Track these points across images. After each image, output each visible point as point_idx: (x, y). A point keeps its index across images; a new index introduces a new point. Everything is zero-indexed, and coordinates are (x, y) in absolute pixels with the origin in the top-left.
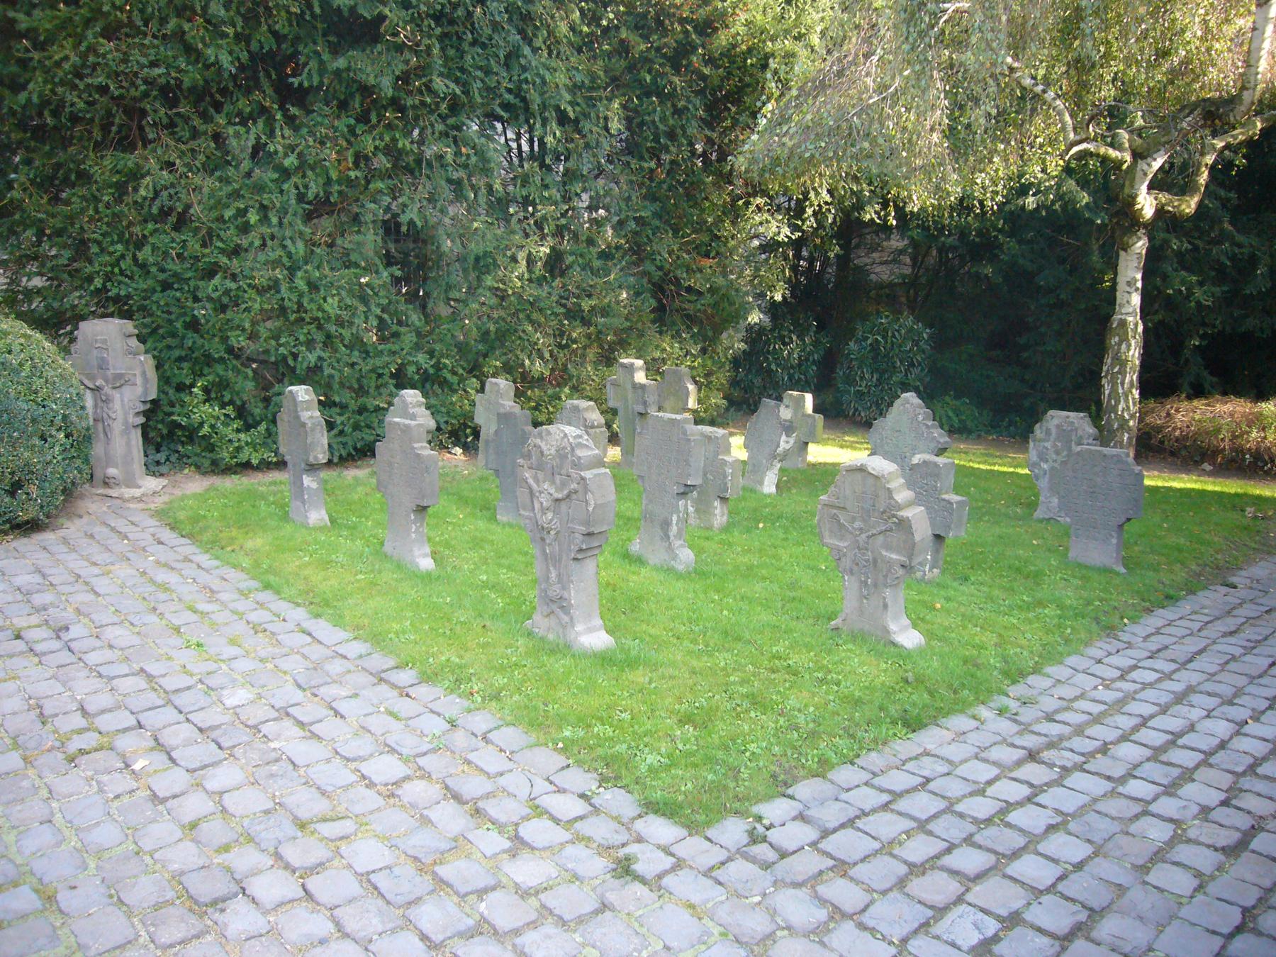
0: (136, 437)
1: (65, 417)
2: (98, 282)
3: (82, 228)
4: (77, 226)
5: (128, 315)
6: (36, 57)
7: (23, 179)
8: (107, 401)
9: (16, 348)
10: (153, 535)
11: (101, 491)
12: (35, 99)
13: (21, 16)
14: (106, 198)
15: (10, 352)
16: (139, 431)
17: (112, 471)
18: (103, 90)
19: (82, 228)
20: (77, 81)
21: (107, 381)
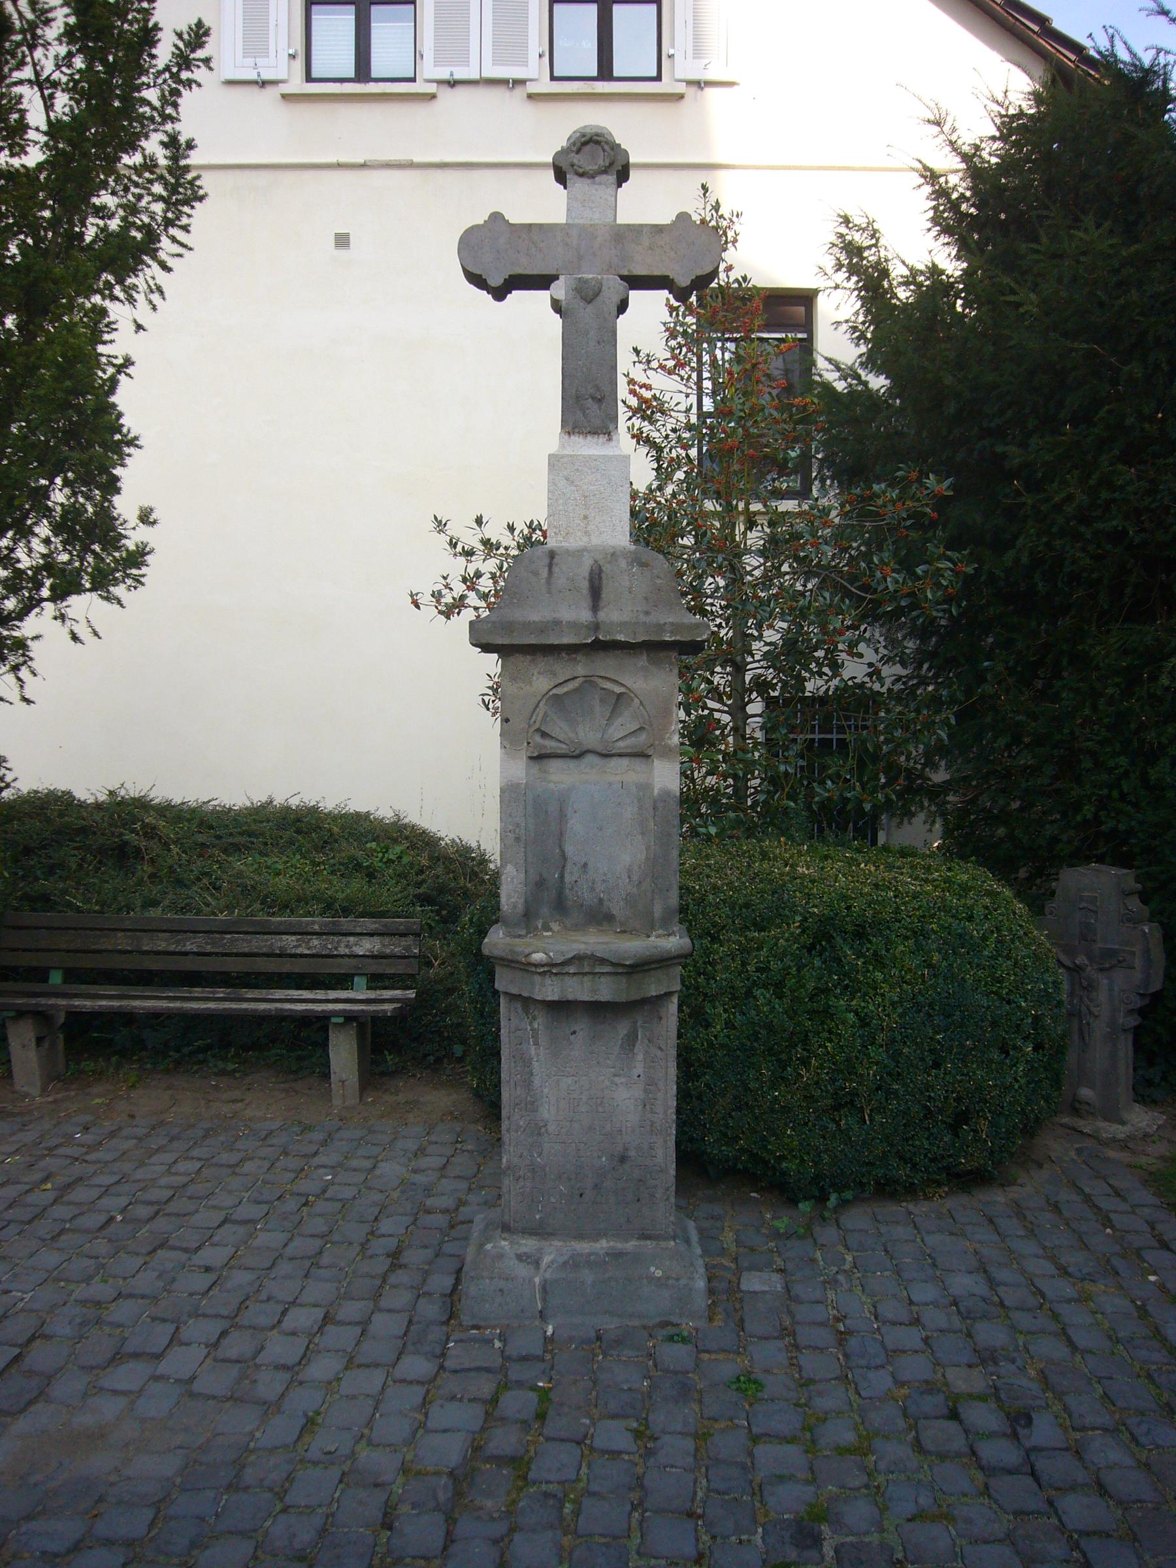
0: (1125, 1048)
1: (1036, 1018)
2: (1088, 811)
3: (1072, 733)
4: (1066, 731)
5: (1123, 861)
6: (1029, 501)
7: (1000, 667)
8: (1090, 987)
9: (979, 911)
10: (1152, 1225)
11: (1066, 1120)
12: (1025, 559)
13: (1012, 449)
14: (1110, 691)
15: (970, 918)
16: (1130, 1037)
17: (1086, 1093)
18: (1118, 536)
19: (1072, 733)
20: (1082, 529)
21: (1091, 959)
